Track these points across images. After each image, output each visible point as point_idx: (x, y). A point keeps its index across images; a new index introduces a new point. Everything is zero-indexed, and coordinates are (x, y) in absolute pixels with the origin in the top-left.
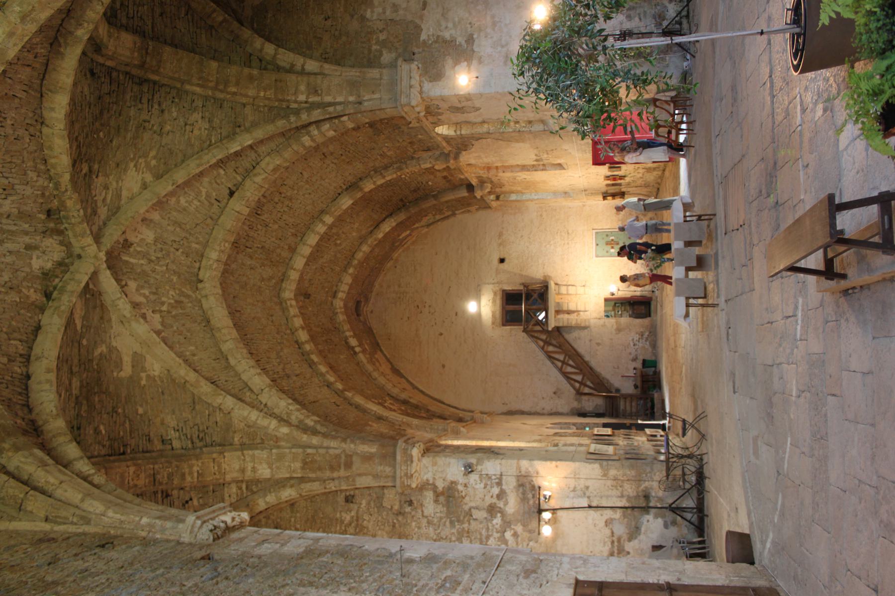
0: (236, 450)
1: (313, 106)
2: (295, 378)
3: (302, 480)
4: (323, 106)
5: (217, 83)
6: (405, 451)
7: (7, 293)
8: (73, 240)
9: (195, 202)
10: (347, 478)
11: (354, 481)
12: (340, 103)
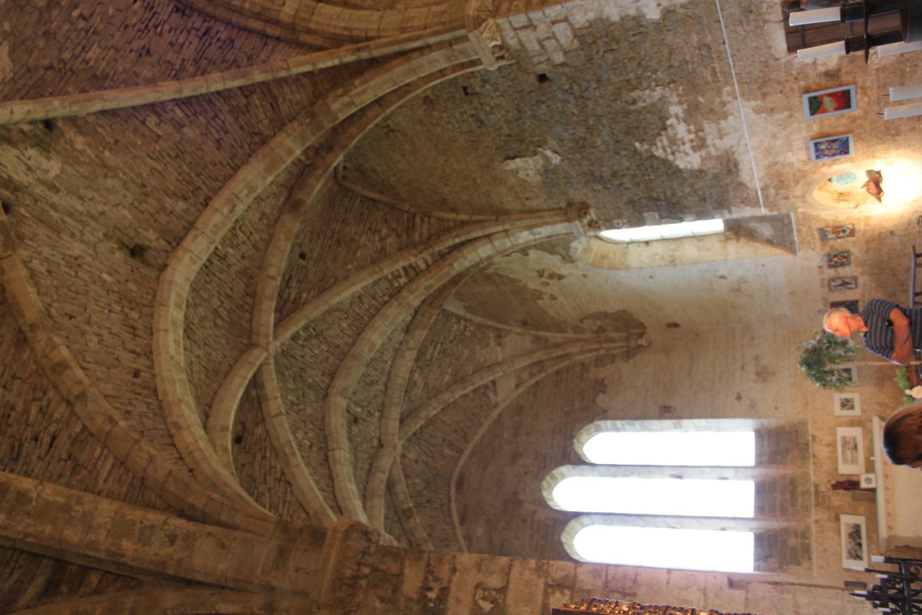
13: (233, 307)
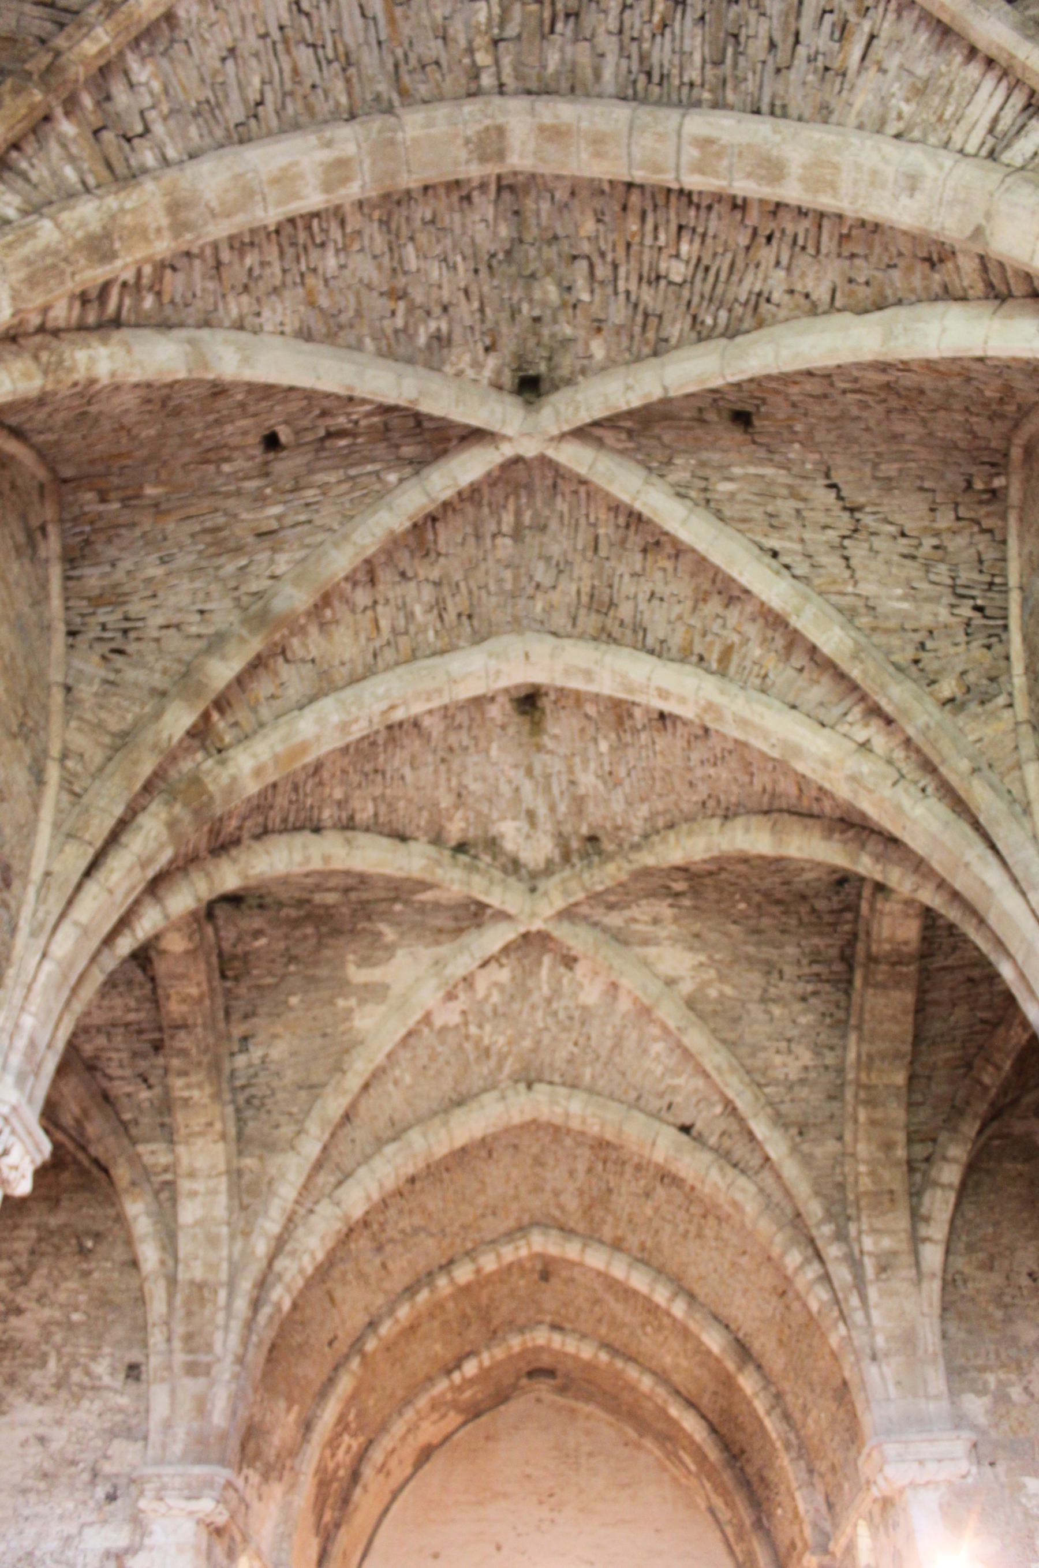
0: (229, 1162)
1: (855, 1263)
2: (377, 1262)
3: (172, 1281)
4: (860, 1284)
5: (868, 1088)
6: (208, 1483)
7: (450, 790)
8: (556, 879)
9: (659, 1070)
10: (169, 1368)
11: (163, 1380)
12: (868, 1317)
13: (486, 510)
